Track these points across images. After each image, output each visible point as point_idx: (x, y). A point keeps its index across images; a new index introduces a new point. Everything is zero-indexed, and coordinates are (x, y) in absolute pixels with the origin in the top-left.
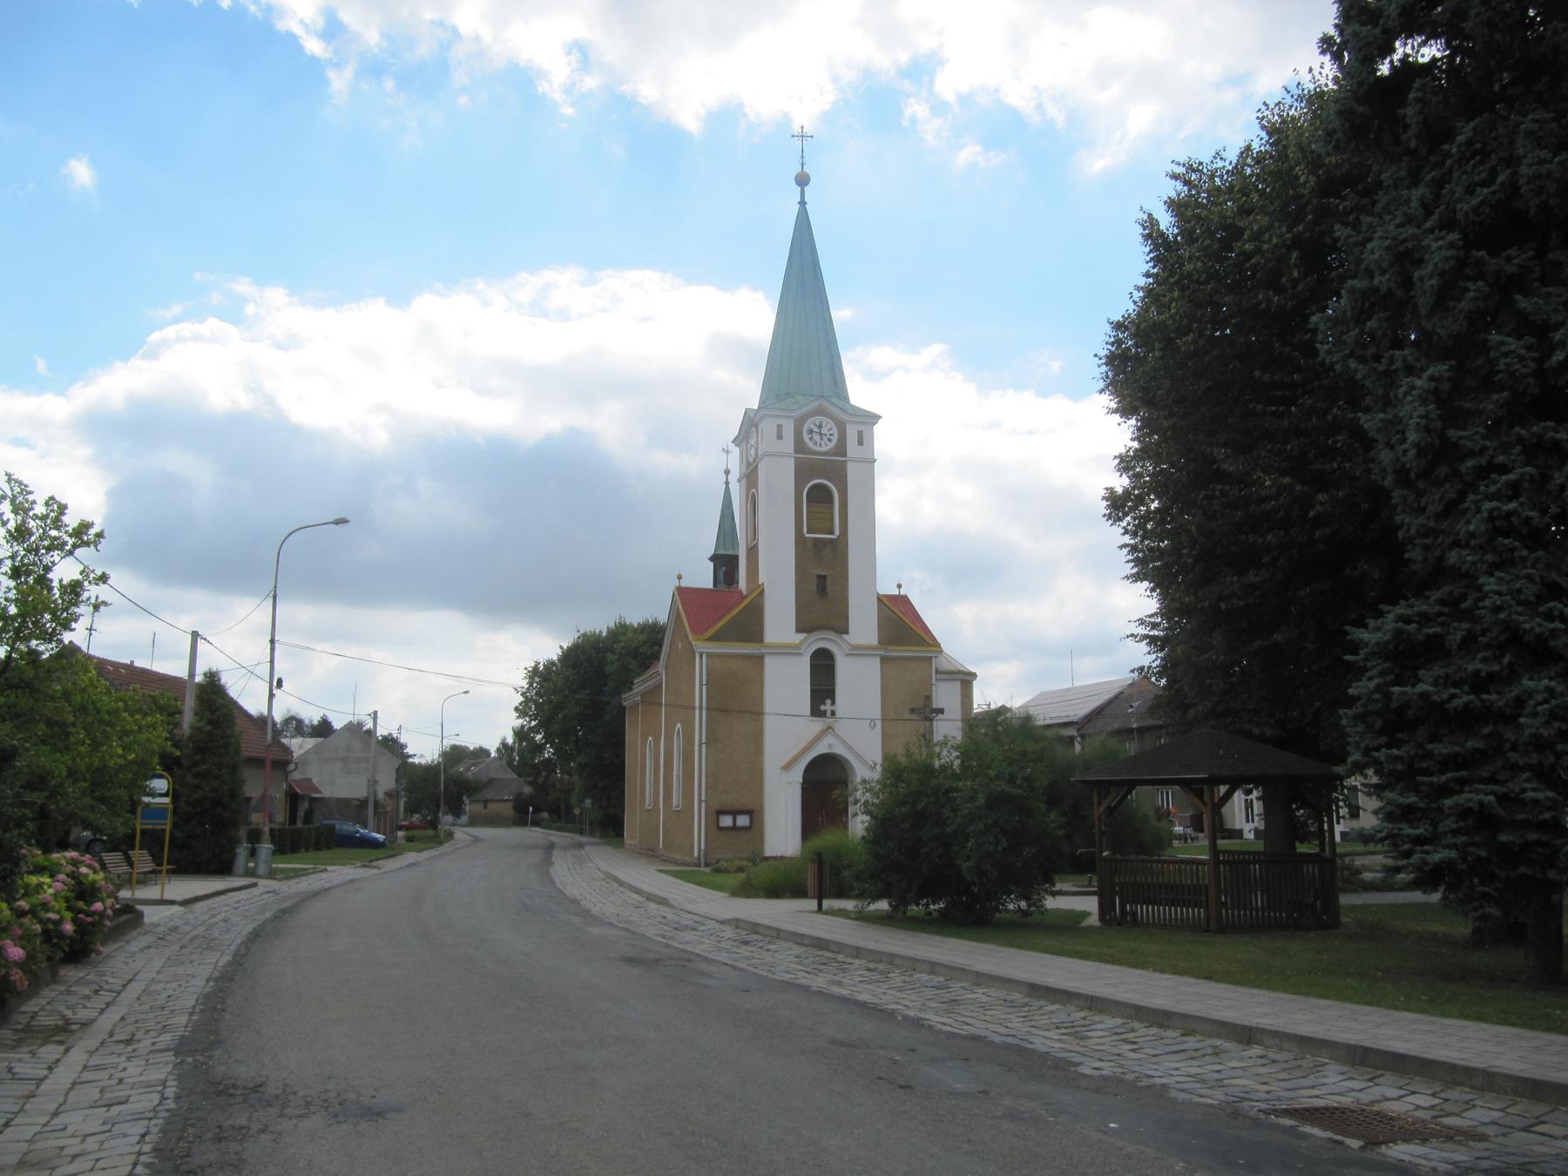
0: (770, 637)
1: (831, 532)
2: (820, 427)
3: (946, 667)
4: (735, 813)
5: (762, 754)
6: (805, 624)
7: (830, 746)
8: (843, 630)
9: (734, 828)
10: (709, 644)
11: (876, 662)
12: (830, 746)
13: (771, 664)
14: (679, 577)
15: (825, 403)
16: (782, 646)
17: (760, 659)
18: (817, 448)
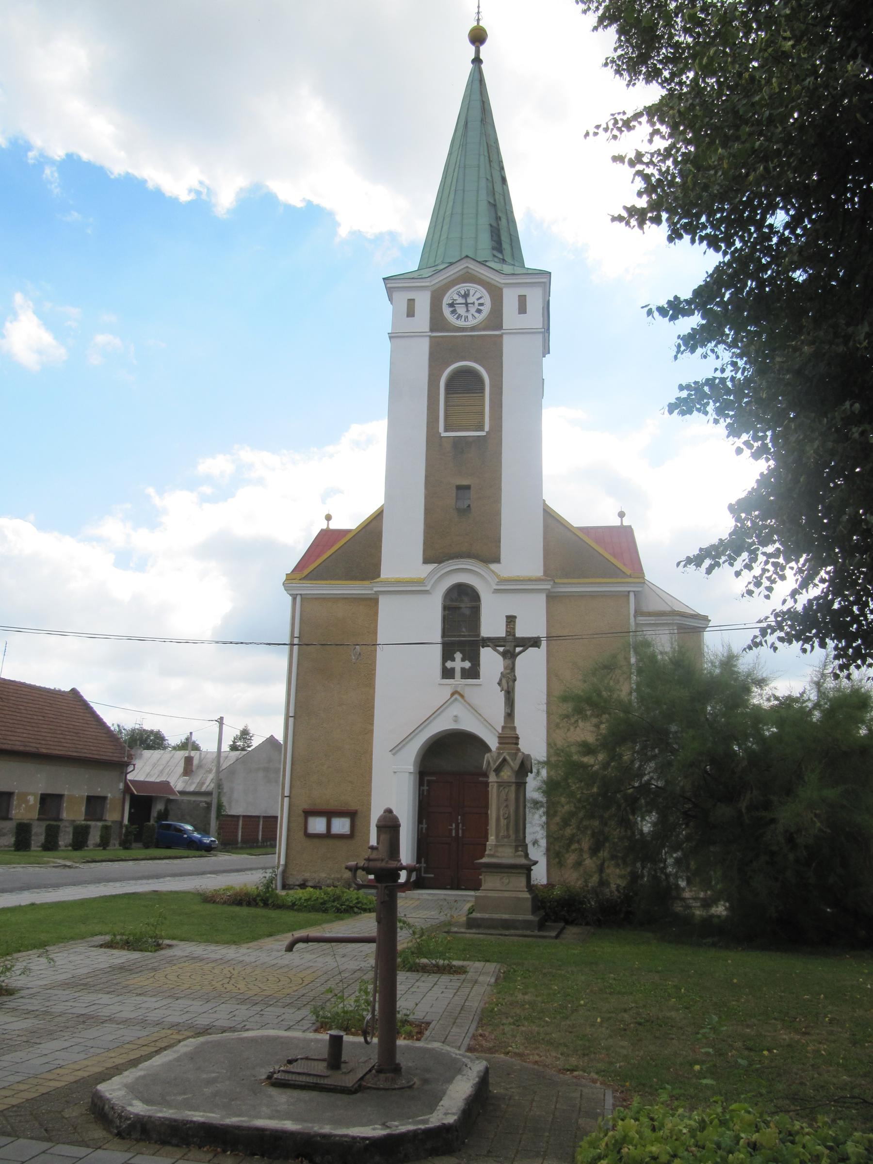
0: (387, 572)
1: (481, 428)
2: (466, 296)
3: (654, 606)
4: (330, 814)
5: (371, 732)
6: (434, 554)
7: (456, 719)
8: (492, 557)
9: (328, 835)
10: (307, 584)
11: (542, 598)
12: (456, 719)
13: (385, 605)
14: (328, 518)
15: (472, 266)
16: (399, 582)
17: (372, 602)
18: (461, 323)
